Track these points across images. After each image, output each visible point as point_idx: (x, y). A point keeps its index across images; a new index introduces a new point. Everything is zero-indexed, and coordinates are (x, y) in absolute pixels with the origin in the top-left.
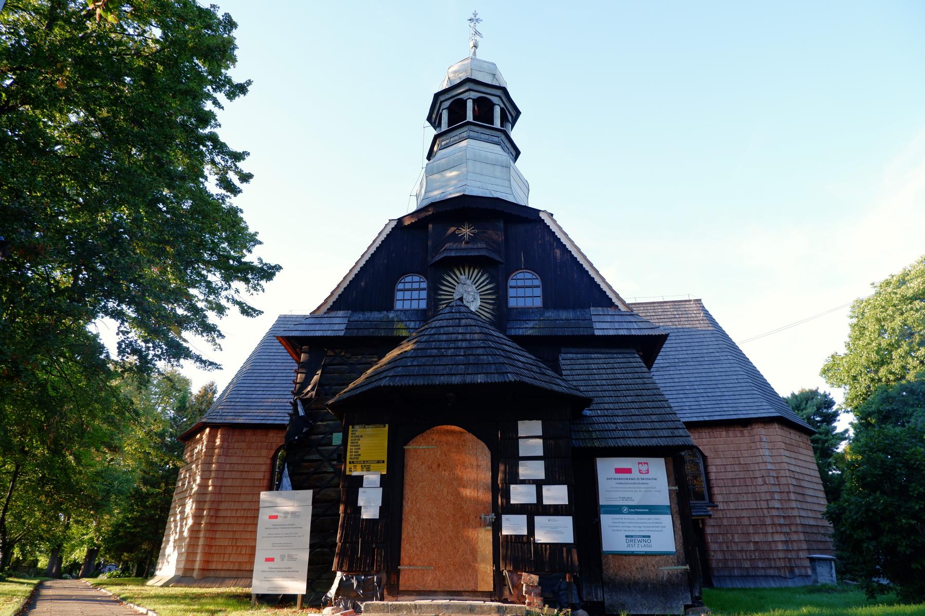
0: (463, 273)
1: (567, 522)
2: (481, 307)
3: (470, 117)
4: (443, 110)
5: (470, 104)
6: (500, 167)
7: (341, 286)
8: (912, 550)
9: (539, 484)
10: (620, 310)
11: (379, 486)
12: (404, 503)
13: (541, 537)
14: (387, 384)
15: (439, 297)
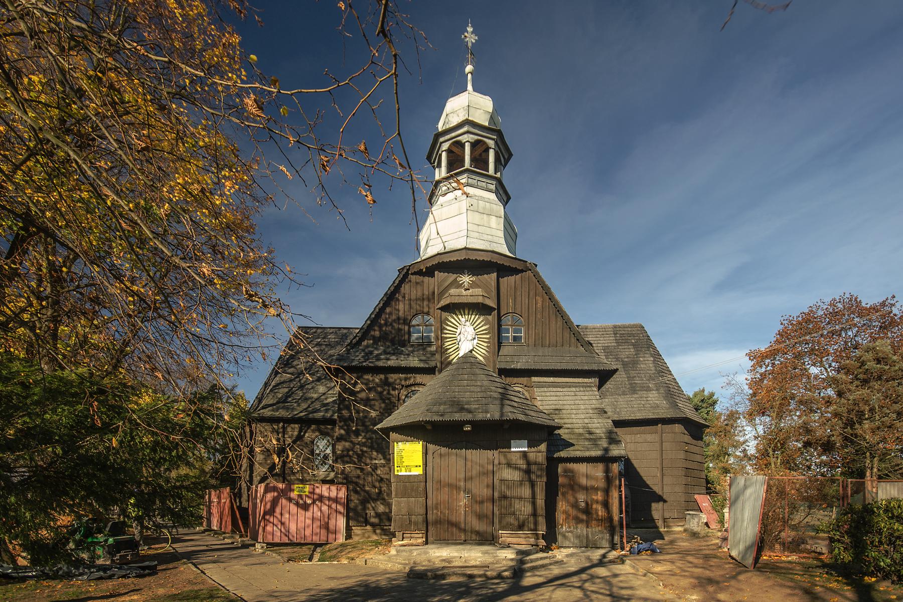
3: (467, 164)
4: (442, 152)
8: (424, 270)
15: (445, 336)
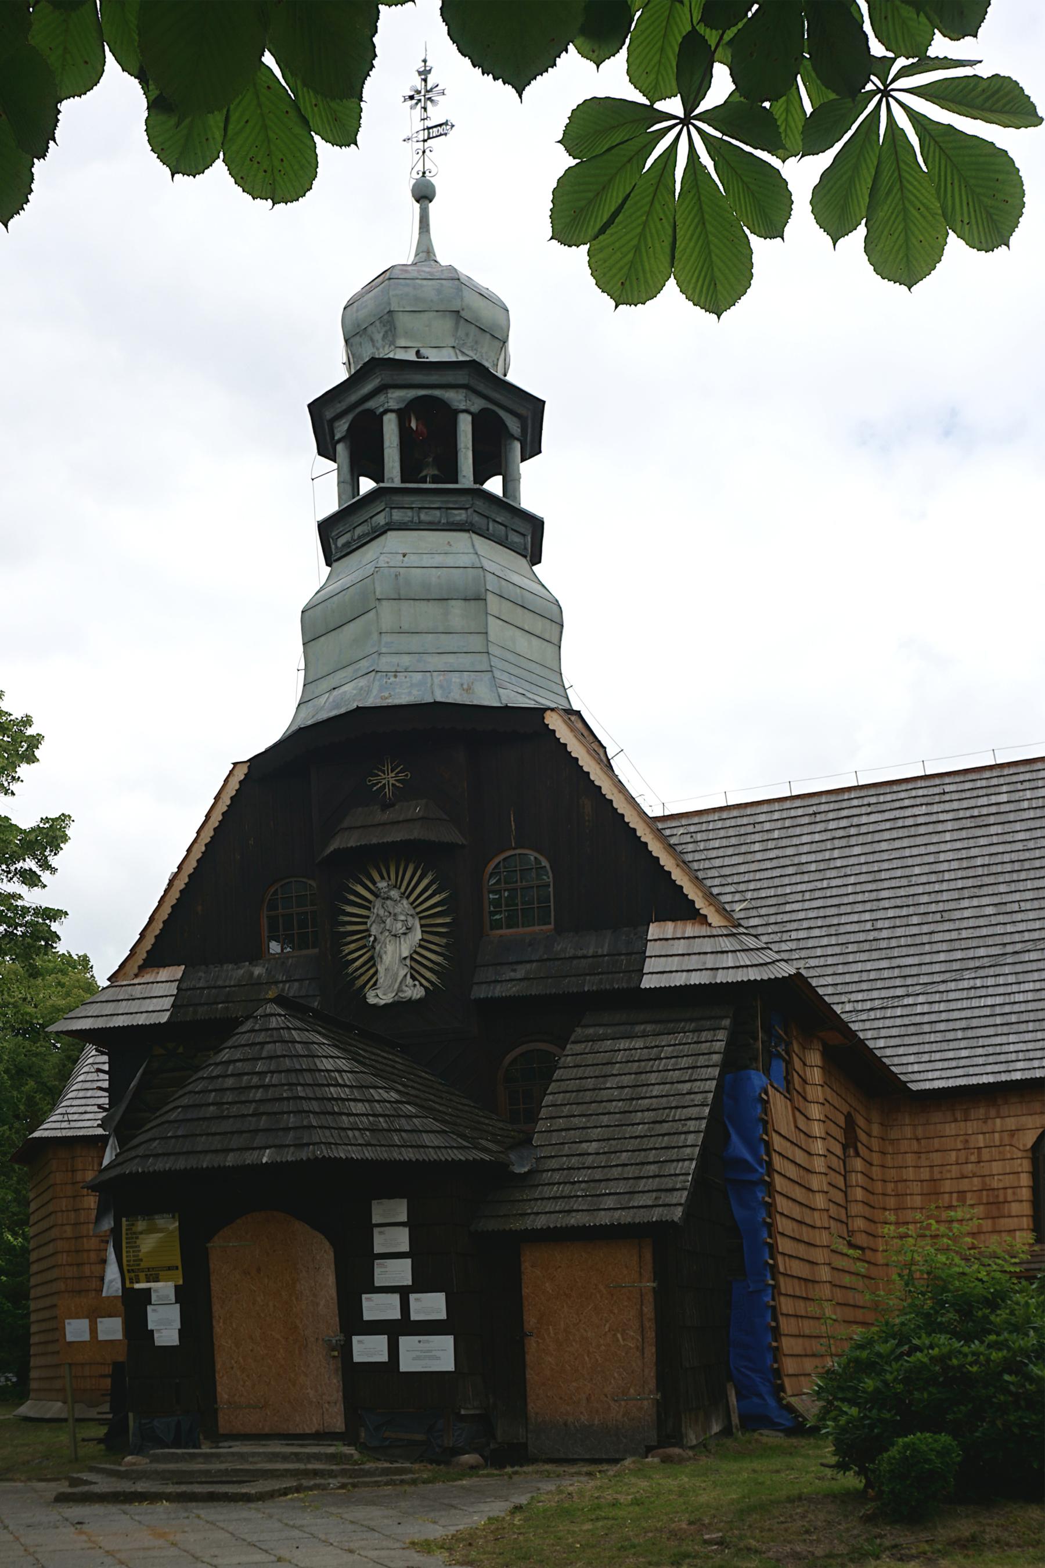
0: (385, 875)
1: (445, 1344)
2: (422, 943)
5: (390, 427)
6: (460, 603)
7: (156, 917)
9: (404, 1293)
10: (710, 925)
11: (173, 1301)
12: (214, 1323)
13: (407, 1364)
14: (134, 1170)
15: (342, 929)
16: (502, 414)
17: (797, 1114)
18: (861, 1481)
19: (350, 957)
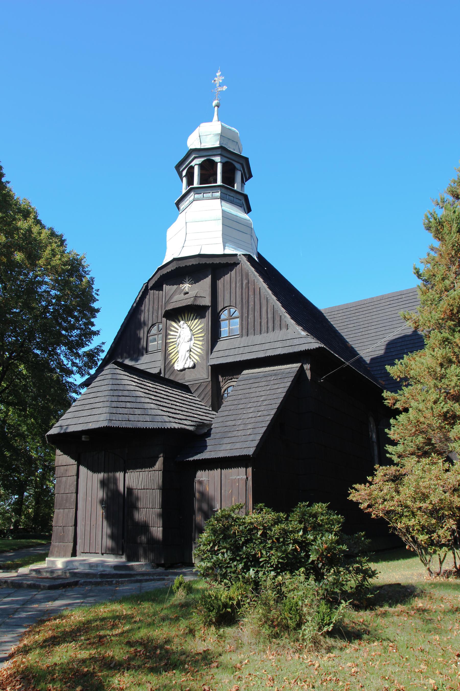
15: (169, 341)
16: (234, 163)
17: (442, 560)
18: (351, 588)
19: (171, 352)
